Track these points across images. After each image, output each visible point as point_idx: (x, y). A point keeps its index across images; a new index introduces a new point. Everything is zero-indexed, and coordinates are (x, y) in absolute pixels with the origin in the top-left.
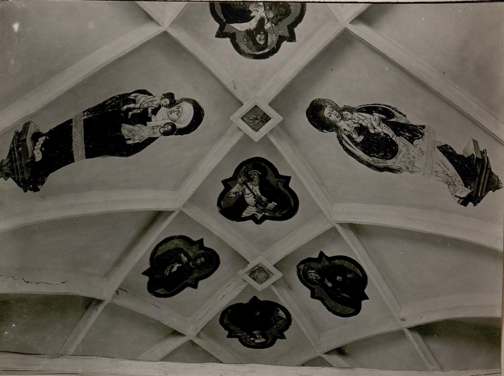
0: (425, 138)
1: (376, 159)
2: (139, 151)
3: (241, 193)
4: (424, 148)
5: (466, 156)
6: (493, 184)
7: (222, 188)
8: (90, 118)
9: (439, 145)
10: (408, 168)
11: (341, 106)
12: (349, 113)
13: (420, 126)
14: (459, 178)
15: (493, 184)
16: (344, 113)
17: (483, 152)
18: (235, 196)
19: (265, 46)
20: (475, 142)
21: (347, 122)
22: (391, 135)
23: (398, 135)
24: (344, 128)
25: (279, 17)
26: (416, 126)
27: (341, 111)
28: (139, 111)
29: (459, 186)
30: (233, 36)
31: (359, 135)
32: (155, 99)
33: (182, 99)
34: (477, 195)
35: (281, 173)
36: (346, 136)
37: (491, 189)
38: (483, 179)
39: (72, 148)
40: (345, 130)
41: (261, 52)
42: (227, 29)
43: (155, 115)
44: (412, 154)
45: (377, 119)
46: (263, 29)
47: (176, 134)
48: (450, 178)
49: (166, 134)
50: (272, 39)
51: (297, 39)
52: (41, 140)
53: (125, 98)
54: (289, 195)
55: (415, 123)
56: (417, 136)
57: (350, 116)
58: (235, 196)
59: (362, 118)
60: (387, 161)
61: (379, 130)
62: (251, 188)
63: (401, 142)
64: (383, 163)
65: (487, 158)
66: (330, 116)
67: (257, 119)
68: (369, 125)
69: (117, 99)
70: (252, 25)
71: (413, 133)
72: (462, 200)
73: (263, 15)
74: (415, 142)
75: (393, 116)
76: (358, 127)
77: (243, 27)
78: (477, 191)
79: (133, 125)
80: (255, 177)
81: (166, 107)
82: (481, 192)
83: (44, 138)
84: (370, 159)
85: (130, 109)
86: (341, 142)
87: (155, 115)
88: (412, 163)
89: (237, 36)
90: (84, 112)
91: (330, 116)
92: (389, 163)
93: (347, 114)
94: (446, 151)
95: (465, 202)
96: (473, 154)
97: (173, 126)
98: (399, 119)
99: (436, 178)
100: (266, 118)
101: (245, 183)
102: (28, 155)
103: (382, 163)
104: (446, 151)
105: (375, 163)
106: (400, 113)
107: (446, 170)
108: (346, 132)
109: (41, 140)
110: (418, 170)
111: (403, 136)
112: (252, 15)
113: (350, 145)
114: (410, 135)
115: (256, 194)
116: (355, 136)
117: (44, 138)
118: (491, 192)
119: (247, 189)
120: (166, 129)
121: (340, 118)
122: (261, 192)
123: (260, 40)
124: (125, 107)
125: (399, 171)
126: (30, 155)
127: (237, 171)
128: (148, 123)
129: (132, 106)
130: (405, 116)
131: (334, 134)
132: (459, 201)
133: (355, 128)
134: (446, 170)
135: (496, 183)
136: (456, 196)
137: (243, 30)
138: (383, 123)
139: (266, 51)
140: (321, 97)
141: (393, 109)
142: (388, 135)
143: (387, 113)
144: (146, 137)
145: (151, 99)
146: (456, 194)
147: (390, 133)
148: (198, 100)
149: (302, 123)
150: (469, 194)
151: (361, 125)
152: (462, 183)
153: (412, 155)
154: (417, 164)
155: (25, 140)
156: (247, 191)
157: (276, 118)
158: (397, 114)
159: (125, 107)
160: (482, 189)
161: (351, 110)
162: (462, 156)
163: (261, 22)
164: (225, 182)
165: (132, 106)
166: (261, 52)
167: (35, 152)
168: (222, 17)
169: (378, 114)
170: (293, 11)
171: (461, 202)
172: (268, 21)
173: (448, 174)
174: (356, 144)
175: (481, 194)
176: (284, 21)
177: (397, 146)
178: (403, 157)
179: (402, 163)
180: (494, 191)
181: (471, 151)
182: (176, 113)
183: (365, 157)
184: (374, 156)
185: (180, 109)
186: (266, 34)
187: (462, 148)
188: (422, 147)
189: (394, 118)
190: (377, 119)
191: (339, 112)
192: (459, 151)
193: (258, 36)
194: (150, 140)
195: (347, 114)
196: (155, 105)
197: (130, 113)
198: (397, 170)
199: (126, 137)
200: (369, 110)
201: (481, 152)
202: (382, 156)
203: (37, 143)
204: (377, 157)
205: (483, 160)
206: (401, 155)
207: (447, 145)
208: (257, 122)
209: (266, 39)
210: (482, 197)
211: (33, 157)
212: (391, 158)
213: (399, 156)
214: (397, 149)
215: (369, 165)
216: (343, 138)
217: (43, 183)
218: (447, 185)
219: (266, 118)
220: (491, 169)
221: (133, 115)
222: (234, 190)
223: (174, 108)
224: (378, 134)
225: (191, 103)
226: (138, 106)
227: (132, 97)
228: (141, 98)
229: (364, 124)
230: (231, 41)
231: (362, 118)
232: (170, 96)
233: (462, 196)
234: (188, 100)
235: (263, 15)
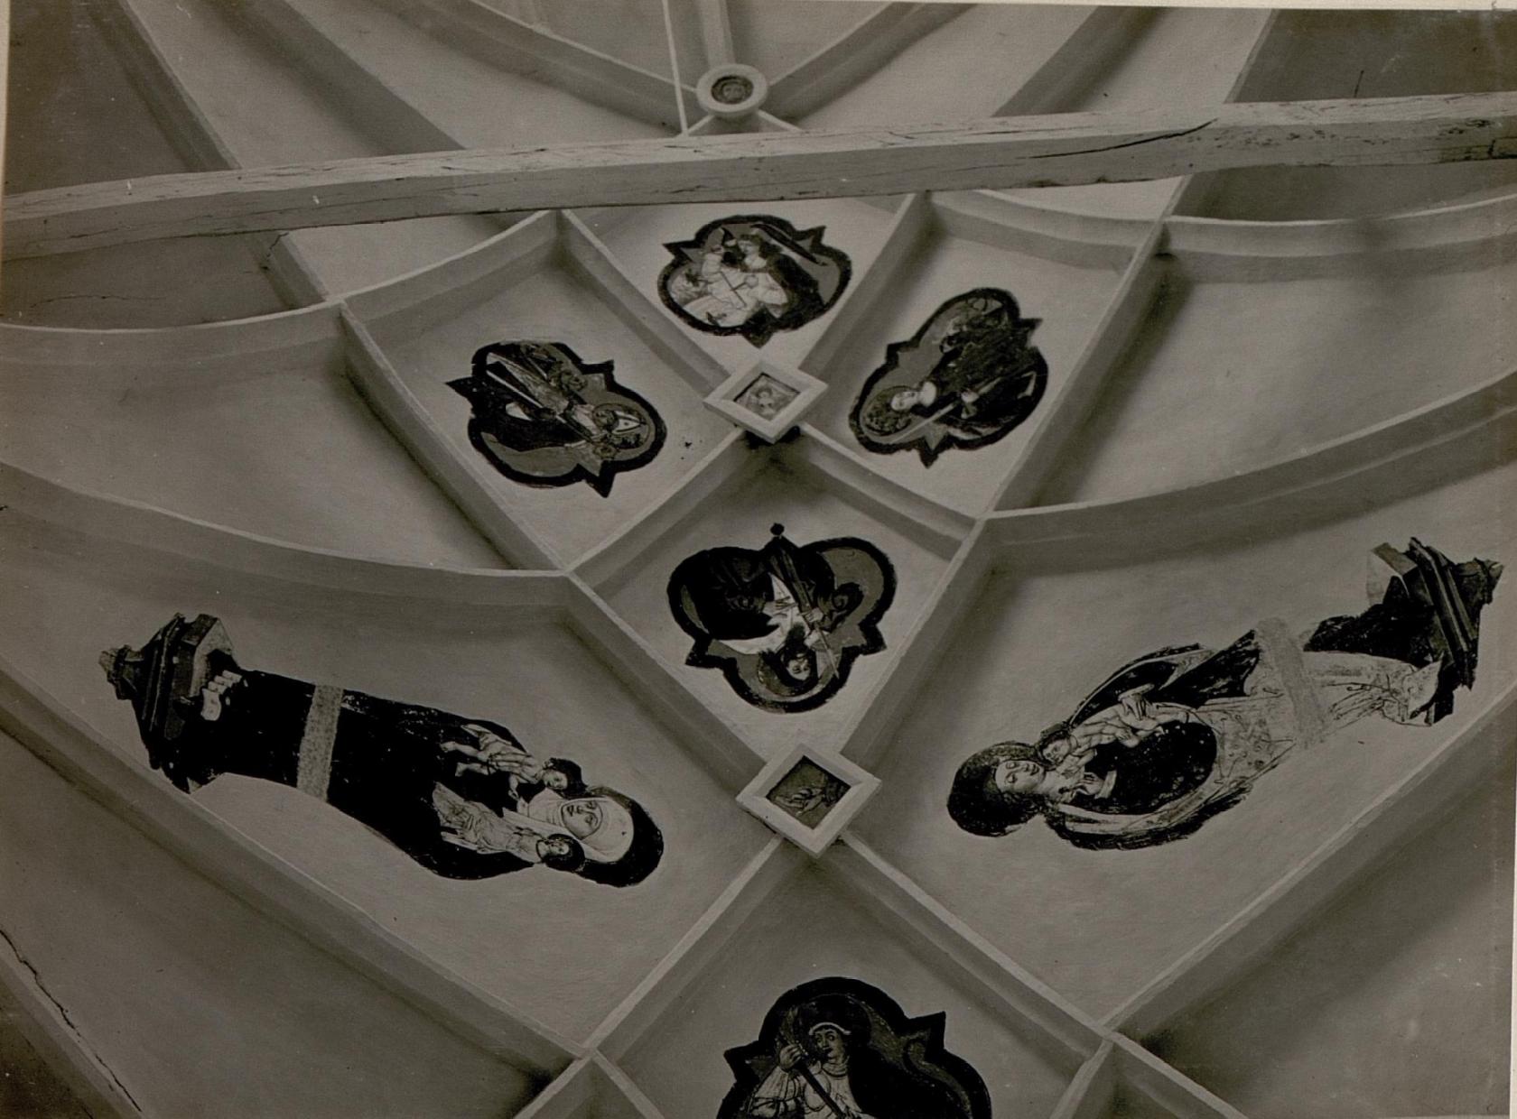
0: (1267, 656)
1: (1167, 806)
2: (473, 876)
3: (791, 1103)
4: (1274, 681)
7: (726, 1080)
8: (355, 713)
9: (1307, 640)
11: (1034, 739)
12: (1058, 743)
13: (1242, 640)
14: (1395, 664)
15: (1476, 585)
16: (1046, 752)
17: (1412, 548)
18: (771, 1113)
19: (813, 680)
20: (1384, 551)
21: (1061, 769)
22: (1181, 717)
23: (1196, 701)
24: (1058, 787)
25: (836, 614)
26: (1234, 647)
27: (1037, 756)
28: (485, 772)
30: (730, 668)
31: (1102, 776)
32: (529, 760)
33: (601, 789)
35: (910, 1013)
36: (1071, 803)
37: (1480, 605)
39: (297, 750)
40: (1062, 791)
41: (803, 697)
42: (714, 648)
43: (528, 800)
44: (1252, 718)
45: (1133, 704)
46: (804, 648)
47: (581, 874)
48: (1374, 690)
49: (552, 861)
50: (827, 662)
51: (886, 641)
52: (229, 678)
53: (452, 725)
54: (950, 1081)
55: (1225, 646)
56: (1243, 669)
57: (1062, 746)
58: (771, 1113)
59: (1095, 729)
60: (1200, 790)
61: (1147, 726)
62: (824, 1085)
63: (1214, 715)
65: (1428, 549)
66: (1014, 780)
67: (811, 797)
68: (1119, 733)
69: (431, 716)
70: (774, 641)
71: (1230, 669)
72: (1433, 708)
73: (800, 619)
75: (1168, 668)
76: (1095, 759)
77: (751, 648)
78: (1454, 643)
79: (467, 799)
80: (833, 1044)
81: (558, 791)
83: (237, 678)
84: (1154, 818)
85: (459, 756)
86: (1063, 832)
87: (528, 800)
88: (1266, 741)
89: (739, 665)
90: (347, 693)
92: (1209, 789)
94: (1336, 636)
97: (576, 848)
98: (1189, 663)
99: (1345, 720)
100: (835, 788)
101: (800, 1068)
102: (188, 687)
103: (1187, 806)
104: (1336, 636)
105: (1172, 816)
106: (1182, 650)
107: (1355, 679)
108: (1067, 794)
109: (229, 678)
110: (1289, 744)
111: (1213, 697)
112: (772, 622)
113: (1088, 821)
114: (1229, 679)
115: (842, 1109)
116: (1091, 789)
117: (237, 678)
119: (810, 1088)
120: (555, 850)
122: (858, 1100)
123: (798, 670)
124: (450, 746)
125: (1242, 791)
126: (193, 692)
127: (773, 1022)
128: (505, 811)
129: (468, 750)
130: (1196, 647)
131: (1039, 819)
132: (1427, 720)
133: (1088, 767)
134: (1355, 679)
135: (1483, 576)
136: (1414, 715)
137: (755, 651)
139: (816, 690)
140: (977, 749)
141: (1162, 654)
142: (1176, 722)
143: (1150, 677)
144: (498, 849)
145: (520, 758)
146: (1411, 710)
147: (1177, 712)
148: (645, 805)
149: (941, 831)
150: (1440, 675)
151: (1099, 747)
152: (1407, 668)
153: (1253, 721)
154: (1276, 733)
155: (193, 650)
156: (813, 1098)
157: (862, 785)
158: (1175, 659)
159: (450, 746)
161: (1061, 732)
162: (1375, 608)
163: (795, 640)
164: (734, 1057)
165: (468, 750)
166: (803, 697)
167: (206, 692)
168: (700, 625)
169: (1130, 692)
170: (866, 593)
172: (812, 627)
174: (1103, 805)
176: (848, 619)
177: (1208, 729)
178: (1235, 746)
179: (1239, 766)
181: (1383, 574)
182: (585, 816)
183: (1137, 823)
184: (1163, 802)
185: (597, 812)
186: (811, 656)
187: (1357, 590)
188: (1270, 683)
189: (1172, 672)
190: (1133, 704)
191: (1035, 758)
192: (1357, 607)
193: (793, 664)
194: (506, 863)
196: (532, 773)
197: (461, 767)
198: (1235, 794)
199: (443, 822)
200: (1105, 698)
201: (1407, 554)
202: (1182, 785)
203: (217, 678)
204: (1170, 799)
205: (1421, 562)
206: (1227, 745)
207: (1324, 623)
208: (812, 803)
209: (813, 666)
210: (1474, 645)
211: (199, 701)
212: (1207, 774)
213: (1225, 751)
214: (1213, 736)
215: (1157, 837)
216: (1064, 815)
217: (203, 781)
218: (1377, 714)
219: (835, 788)
220: (1450, 563)
221: (467, 772)
222: (768, 1090)
223: (581, 802)
224: (1150, 740)
225: (627, 806)
226: (483, 756)
227: (471, 729)
228: (494, 744)
229: (1105, 741)
230: (727, 676)
231: (1095, 729)
232: (571, 770)
233: (1426, 700)
234: (618, 797)
235: (800, 619)
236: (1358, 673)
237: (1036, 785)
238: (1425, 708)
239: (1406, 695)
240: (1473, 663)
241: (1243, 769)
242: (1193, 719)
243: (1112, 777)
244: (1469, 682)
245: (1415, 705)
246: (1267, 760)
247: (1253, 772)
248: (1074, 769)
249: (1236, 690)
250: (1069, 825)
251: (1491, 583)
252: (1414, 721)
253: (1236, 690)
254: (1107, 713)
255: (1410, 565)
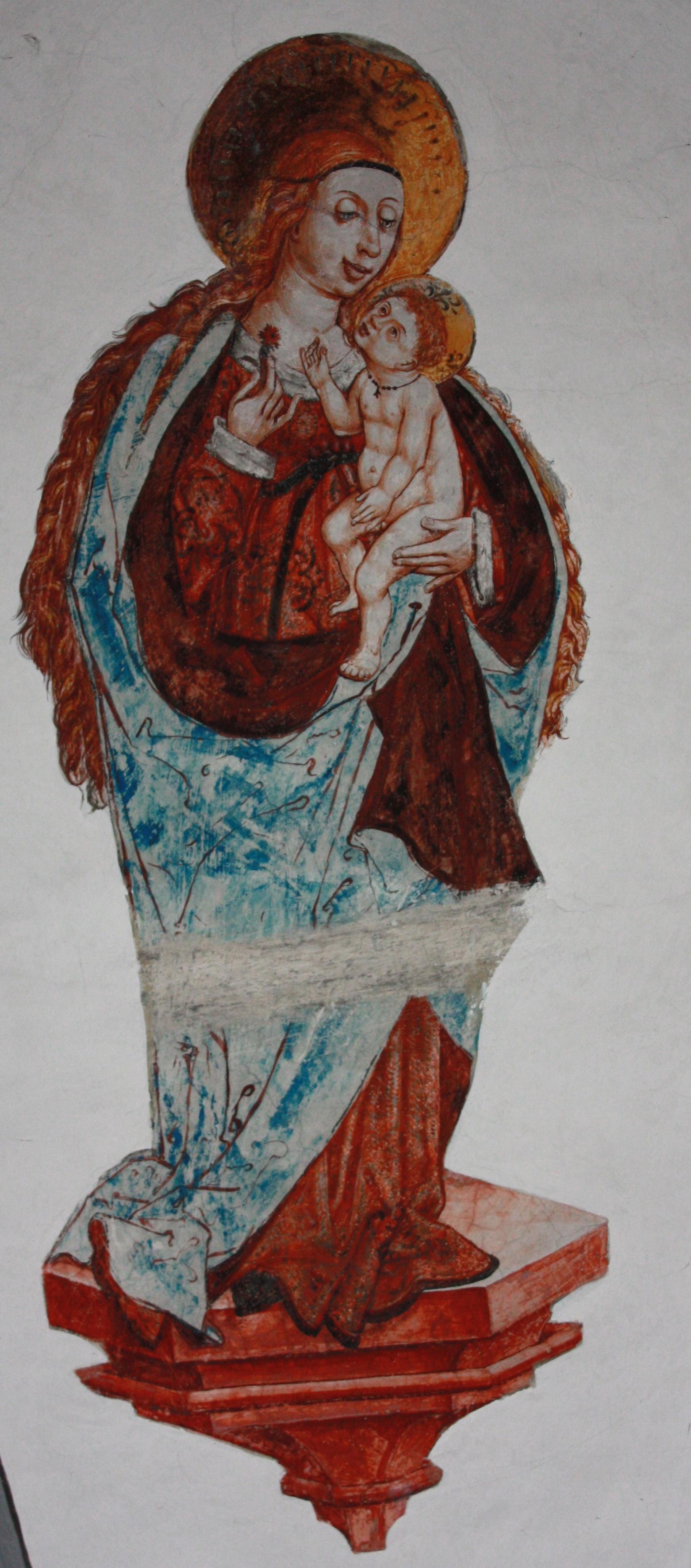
5: (454, 1214)
6: (354, 1470)
10: (148, 833)
12: (411, 339)
15: (354, 1470)
22: (364, 660)
23: (384, 706)
29: (185, 1232)
34: (195, 1377)
38: (343, 1385)
40: (270, 336)
44: (284, 840)
45: (445, 545)
48: (214, 1149)
59: (414, 440)
63: (334, 750)
64: (113, 647)
68: (376, 500)
71: (456, 815)
72: (89, 1280)
74: (381, 843)
82: (235, 1405)
84: (108, 557)
91: (340, 216)
92: (136, 705)
93: (396, 331)
95: (78, 1299)
96: (494, 1263)
108: (251, 346)
110: (171, 915)
113: (160, 393)
116: (248, 414)
118: (271, 1471)
121: (349, 288)
132: (66, 1259)
133: (316, 407)
134: (269, 1108)
136: (97, 1233)
138: (436, 592)
143: (522, 590)
146: (113, 1228)
147: (377, 655)
150: (169, 1318)
151: (356, 444)
153: (274, 838)
158: (538, 675)
160: (255, 1403)
169: (485, 541)
171: (72, 1275)
173: (239, 1126)
174: (545, 714)
175: (217, 1407)
180: (289, 1488)
183: (109, 519)
189: (504, 654)
190: (445, 545)
195: (396, 331)
205: (492, 1345)
206: (236, 765)
212: (181, 705)
229: (370, 461)
231: (414, 440)
236: (279, 1120)
237: (311, 269)
238: (100, 1262)
239: (161, 1225)
240: (148, 1408)
241: (155, 794)
242: (344, 689)
243: (258, 465)
244: (96, 1381)
245: (121, 1240)
246: (151, 855)
247: (138, 814)
248: (320, 373)
249: (383, 808)
250: (164, 345)
251: (332, 1510)
252: (82, 1225)
253: (383, 808)
254: (449, 474)
255: (505, 1308)
